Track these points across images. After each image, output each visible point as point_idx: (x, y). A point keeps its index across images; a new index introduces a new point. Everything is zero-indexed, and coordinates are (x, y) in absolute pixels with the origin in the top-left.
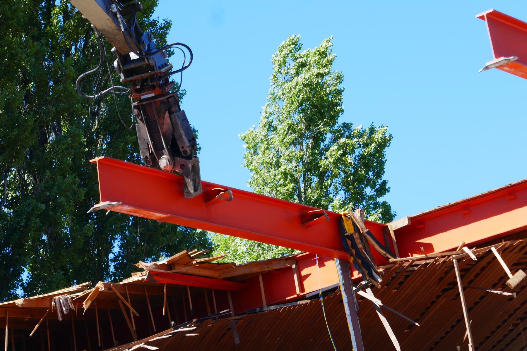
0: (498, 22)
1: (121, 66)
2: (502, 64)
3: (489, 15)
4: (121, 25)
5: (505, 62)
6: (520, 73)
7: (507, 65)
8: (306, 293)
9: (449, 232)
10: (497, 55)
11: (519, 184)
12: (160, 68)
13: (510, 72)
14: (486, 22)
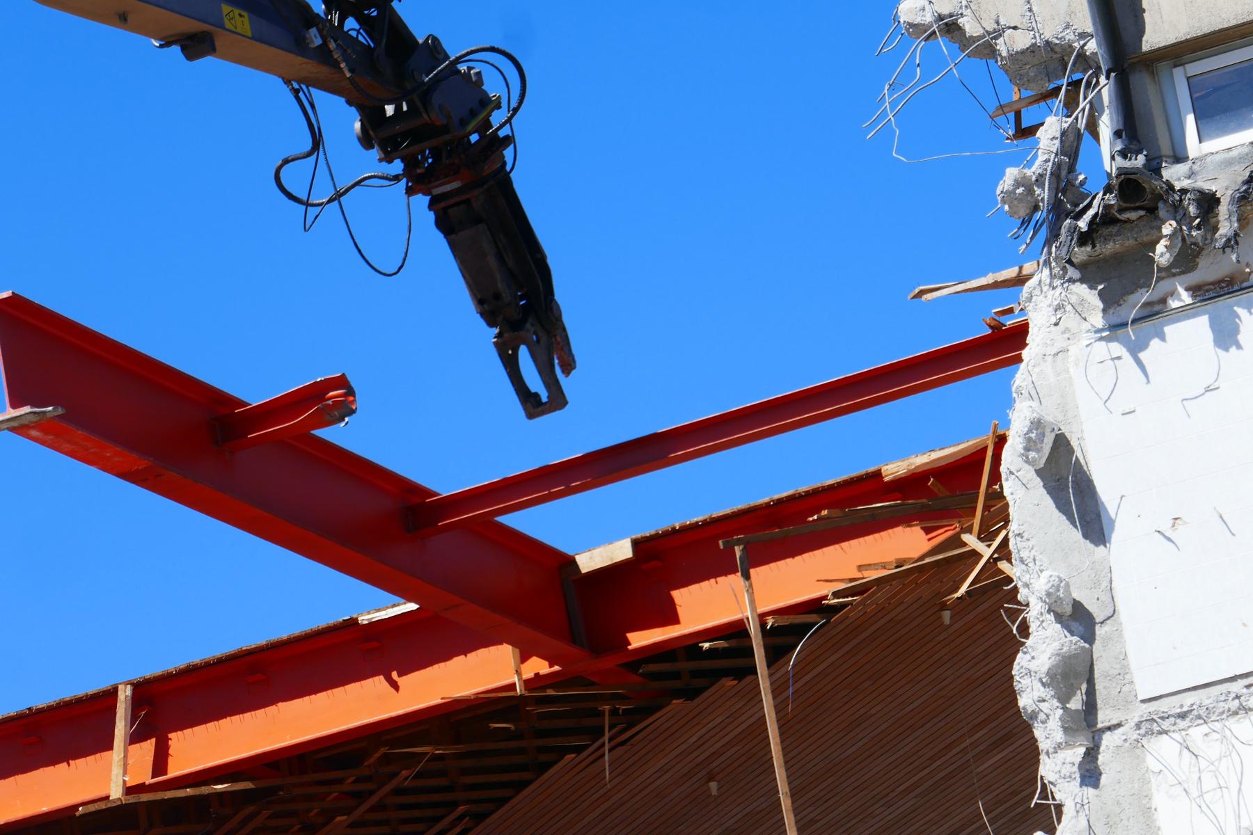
1: (371, 133)
2: (25, 421)
5: (34, 418)
7: (37, 426)
8: (516, 679)
10: (15, 405)
13: (43, 443)
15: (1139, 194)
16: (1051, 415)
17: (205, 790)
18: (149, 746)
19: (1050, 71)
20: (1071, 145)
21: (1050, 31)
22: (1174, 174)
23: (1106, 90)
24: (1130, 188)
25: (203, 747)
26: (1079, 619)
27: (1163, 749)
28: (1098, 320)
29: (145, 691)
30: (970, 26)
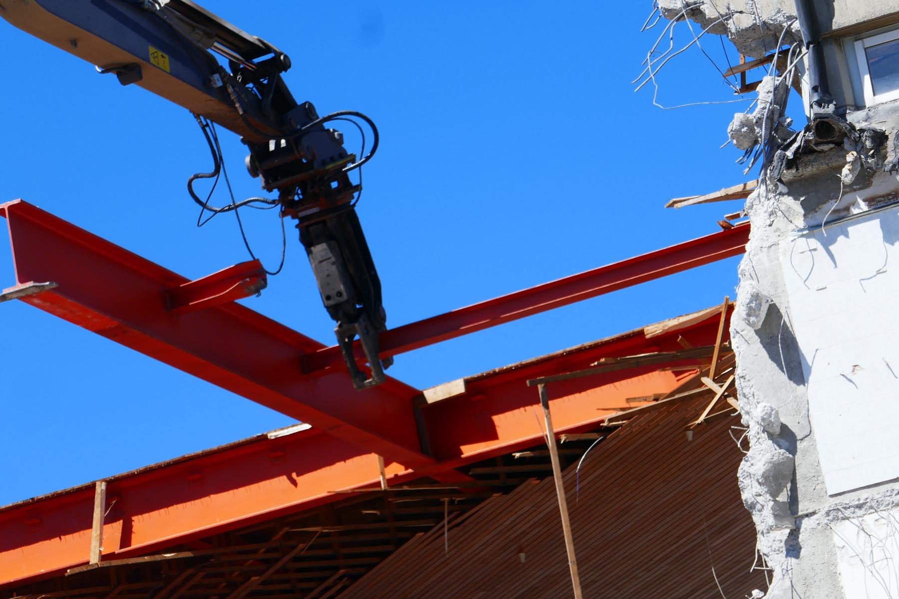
2: (29, 292)
4: (237, 105)
7: (39, 296)
9: (349, 462)
10: (22, 280)
13: (42, 308)
15: (830, 133)
17: (158, 558)
18: (118, 526)
19: (766, 43)
20: (781, 96)
21: (767, 14)
22: (855, 118)
23: (806, 57)
24: (823, 128)
25: (157, 527)
26: (785, 437)
27: (845, 530)
28: (800, 222)
29: (115, 486)
30: (709, 11)
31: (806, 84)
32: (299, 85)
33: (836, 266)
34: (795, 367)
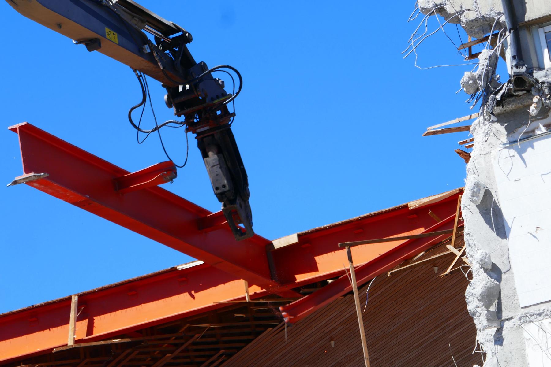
0: (31, 136)
2: (31, 179)
3: (21, 127)
4: (159, 64)
5: (35, 178)
6: (50, 190)
7: (37, 181)
10: (27, 172)
11: (42, 306)
12: (212, 99)
14: (18, 135)
15: (523, 84)
16: (483, 181)
17: (109, 342)
19: (484, 29)
20: (493, 62)
21: (485, 12)
22: (538, 75)
23: (509, 37)
24: (519, 81)
26: (494, 271)
27: (531, 329)
28: (504, 139)
29: (84, 299)
30: (449, 9)
31: (509, 54)
32: (197, 51)
33: (526, 166)
34: (500, 228)
